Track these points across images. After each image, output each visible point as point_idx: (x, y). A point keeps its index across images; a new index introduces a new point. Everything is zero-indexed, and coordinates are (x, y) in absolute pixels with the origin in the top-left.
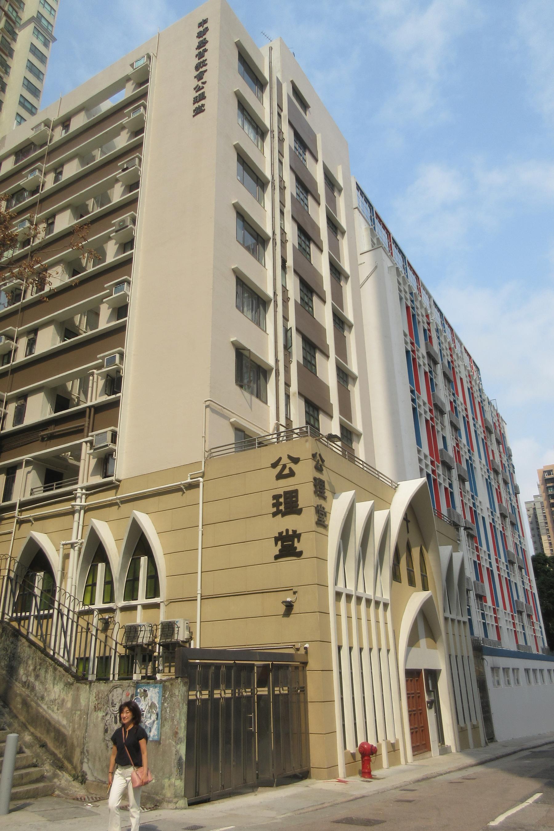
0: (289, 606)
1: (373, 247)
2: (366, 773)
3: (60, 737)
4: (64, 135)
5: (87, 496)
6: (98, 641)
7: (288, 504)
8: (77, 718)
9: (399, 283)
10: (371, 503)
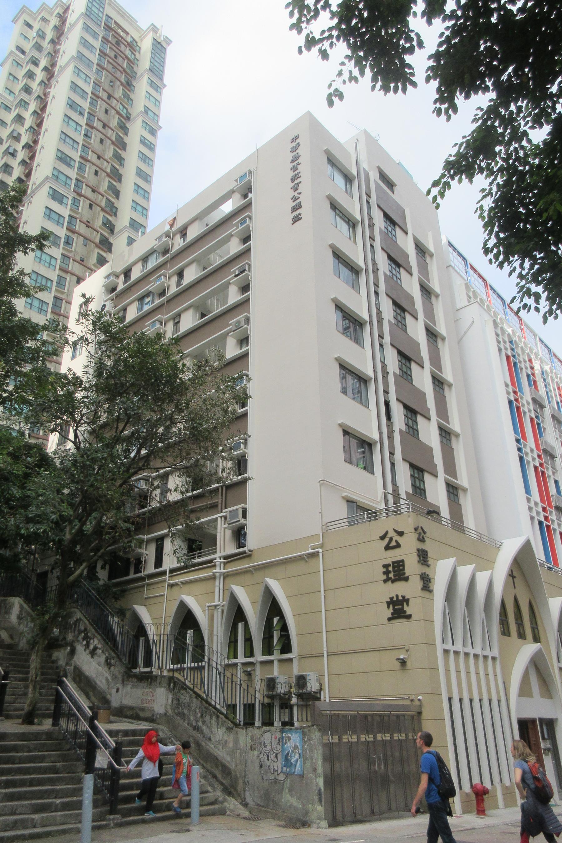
0: (403, 663)
1: (469, 301)
2: (481, 812)
3: (226, 770)
4: (182, 244)
5: (225, 564)
6: (242, 689)
7: (396, 572)
8: (238, 756)
9: (497, 335)
10: (473, 566)
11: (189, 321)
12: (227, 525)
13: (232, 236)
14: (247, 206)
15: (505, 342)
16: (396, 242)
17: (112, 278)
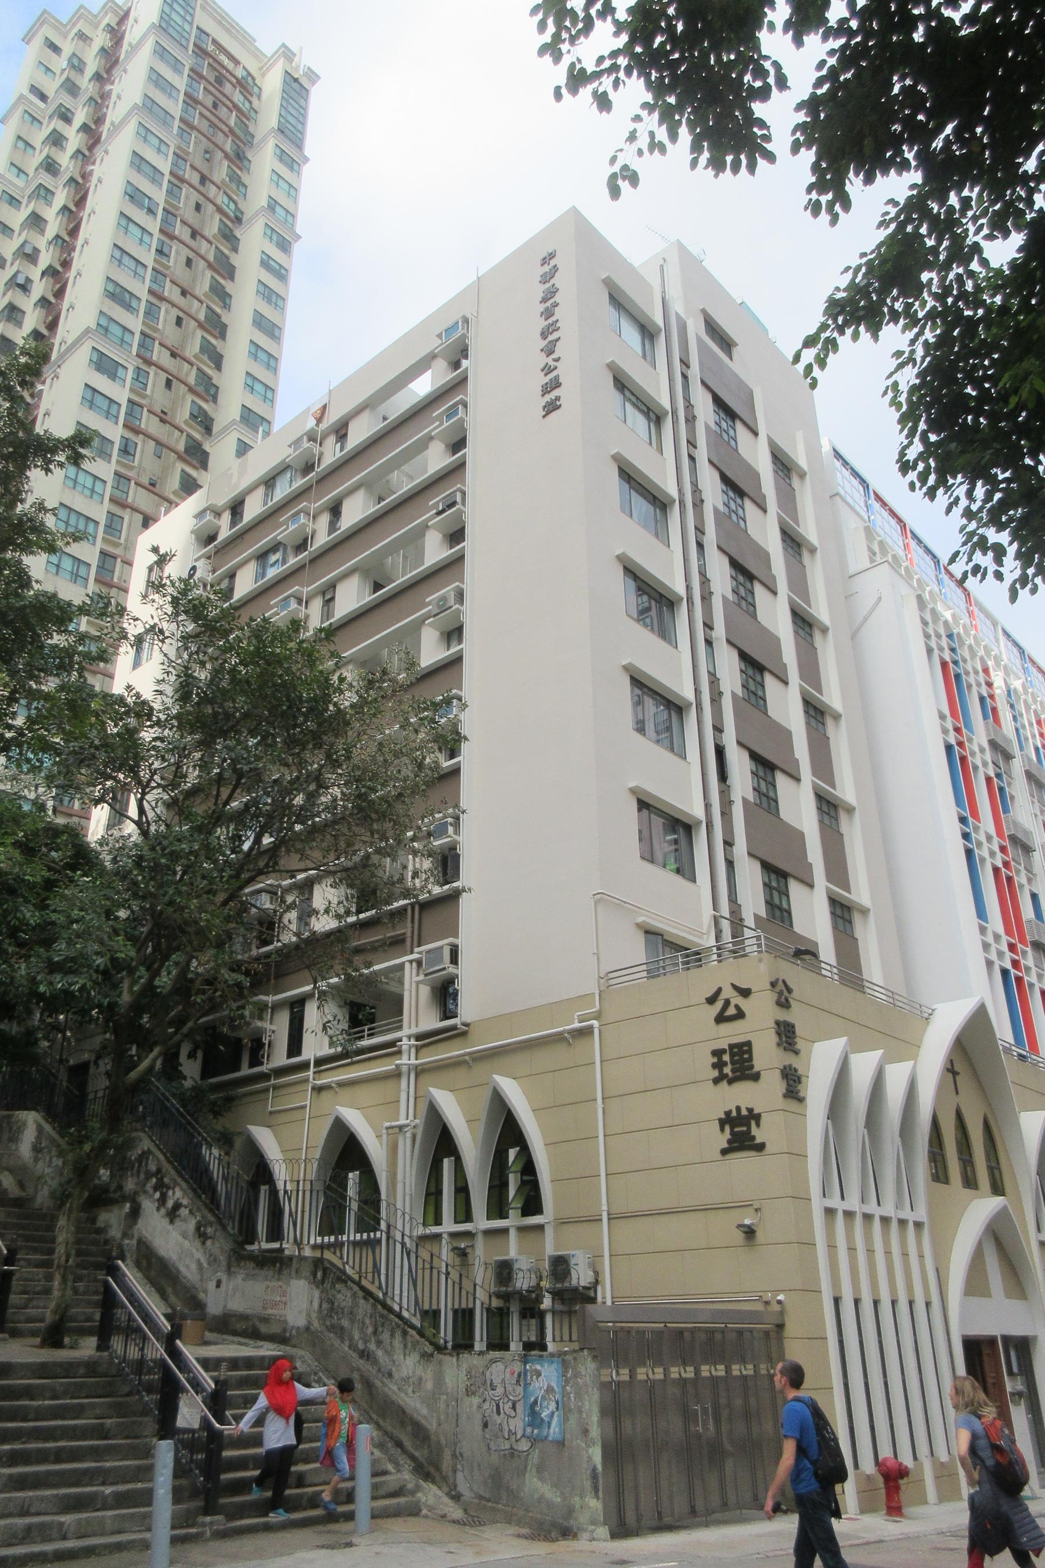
0: (750, 1232)
1: (872, 561)
2: (894, 1509)
3: (420, 1433)
4: (338, 455)
5: (418, 1049)
6: (450, 1282)
7: (736, 1064)
8: (442, 1406)
9: (925, 623)
10: (879, 1053)
11: (351, 597)
12: (421, 977)
13: (431, 438)
14: (460, 383)
15: (938, 636)
16: (736, 450)
17: (209, 517)
